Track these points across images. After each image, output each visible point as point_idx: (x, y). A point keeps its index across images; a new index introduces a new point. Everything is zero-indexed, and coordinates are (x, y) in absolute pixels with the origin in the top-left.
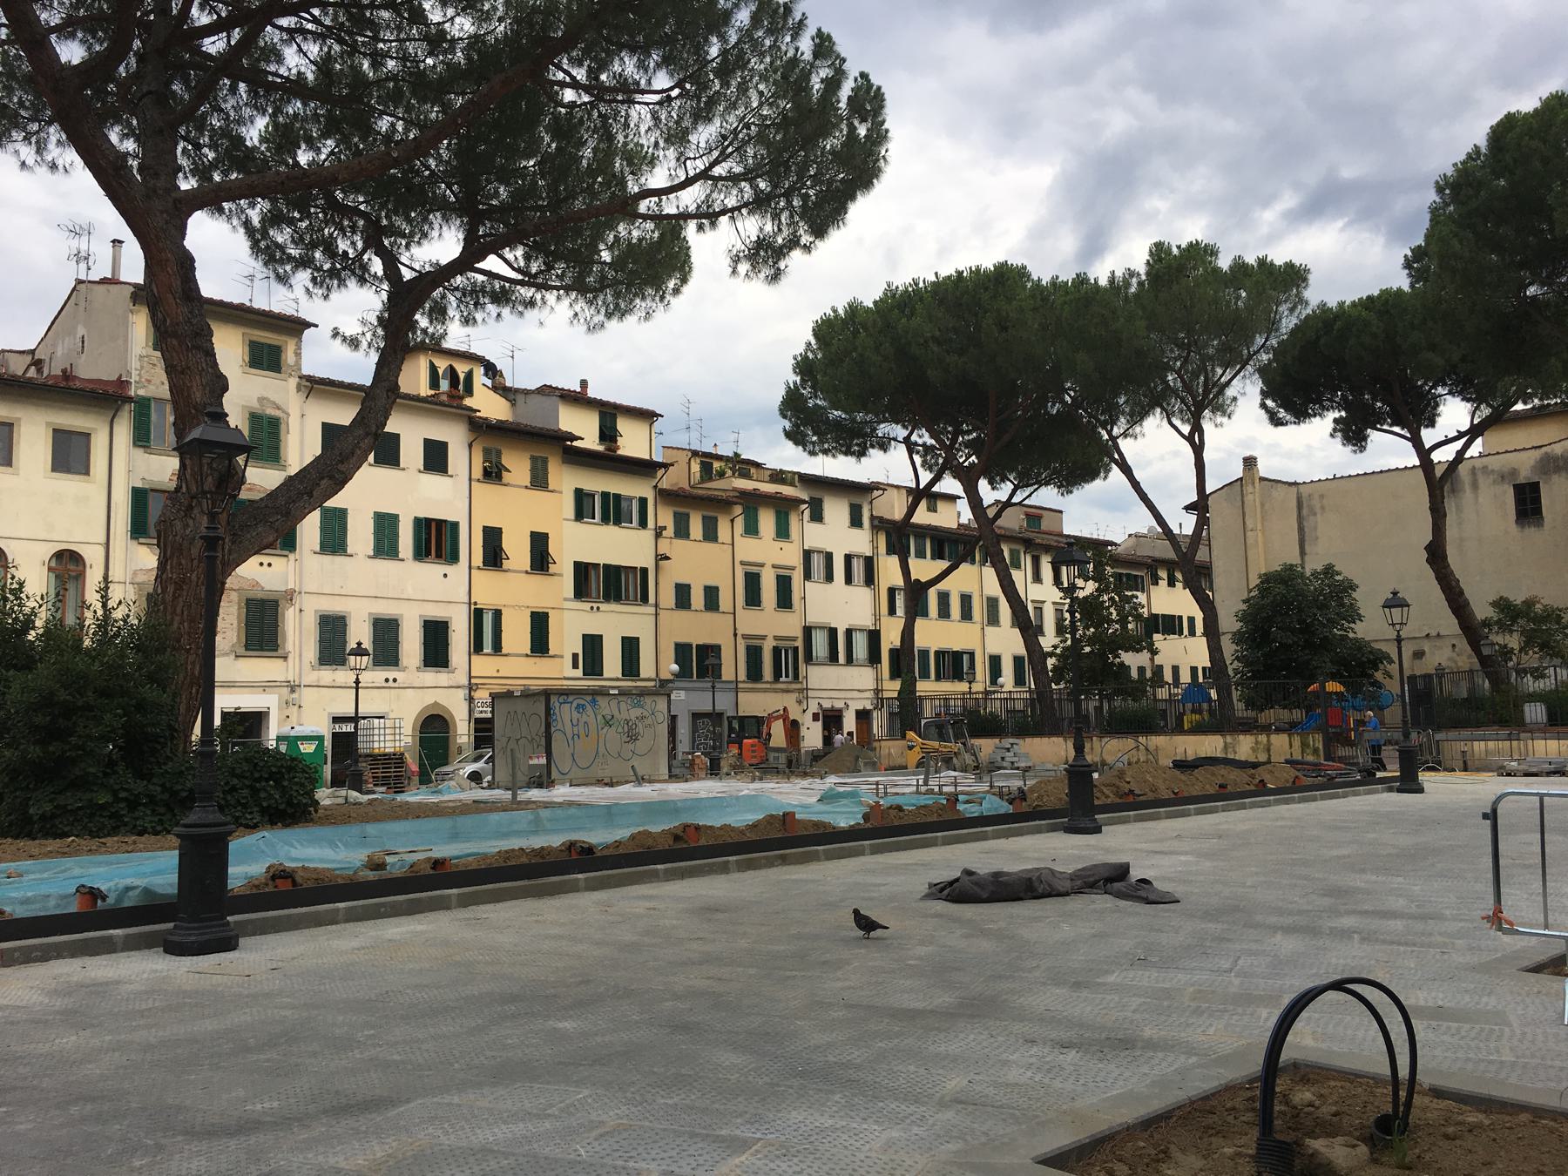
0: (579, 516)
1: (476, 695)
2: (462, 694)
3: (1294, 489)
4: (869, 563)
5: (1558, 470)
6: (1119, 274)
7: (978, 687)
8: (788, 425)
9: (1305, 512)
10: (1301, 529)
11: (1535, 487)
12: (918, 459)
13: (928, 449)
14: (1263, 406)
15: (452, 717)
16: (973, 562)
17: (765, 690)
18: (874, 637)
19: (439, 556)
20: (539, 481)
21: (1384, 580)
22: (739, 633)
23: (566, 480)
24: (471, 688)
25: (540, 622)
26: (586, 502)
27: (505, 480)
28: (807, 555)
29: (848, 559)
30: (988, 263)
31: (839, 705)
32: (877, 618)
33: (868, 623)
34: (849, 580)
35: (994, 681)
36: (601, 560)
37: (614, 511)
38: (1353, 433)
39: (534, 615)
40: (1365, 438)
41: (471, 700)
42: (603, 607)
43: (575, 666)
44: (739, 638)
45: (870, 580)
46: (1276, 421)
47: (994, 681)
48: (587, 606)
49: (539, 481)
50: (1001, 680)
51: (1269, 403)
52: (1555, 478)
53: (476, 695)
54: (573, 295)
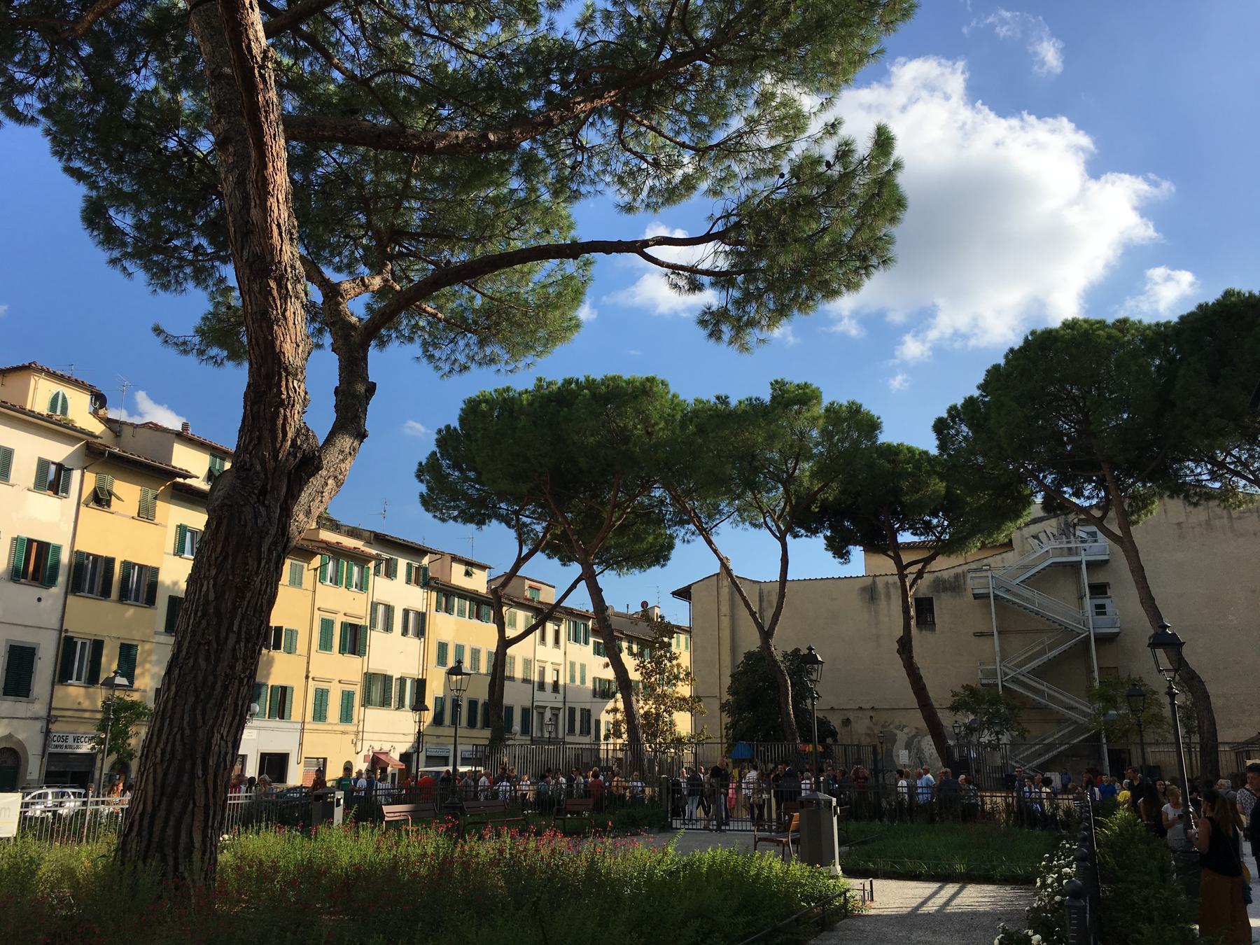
0: (1105, 613)
1: (53, 727)
2: (39, 726)
3: (757, 587)
4: (421, 618)
5: (945, 590)
11: (930, 601)
15: (26, 752)
17: (327, 731)
18: (420, 685)
19: (91, 591)
20: (146, 513)
21: (857, 671)
22: (311, 675)
24: (50, 719)
27: (113, 509)
28: (374, 606)
29: (406, 612)
30: (332, 400)
31: (386, 748)
32: (424, 669)
33: (414, 671)
34: (405, 632)
38: (839, 548)
39: (123, 646)
40: (848, 553)
41: (47, 733)
45: (421, 632)
49: (146, 513)
52: (943, 595)
53: (53, 727)
54: (743, 199)
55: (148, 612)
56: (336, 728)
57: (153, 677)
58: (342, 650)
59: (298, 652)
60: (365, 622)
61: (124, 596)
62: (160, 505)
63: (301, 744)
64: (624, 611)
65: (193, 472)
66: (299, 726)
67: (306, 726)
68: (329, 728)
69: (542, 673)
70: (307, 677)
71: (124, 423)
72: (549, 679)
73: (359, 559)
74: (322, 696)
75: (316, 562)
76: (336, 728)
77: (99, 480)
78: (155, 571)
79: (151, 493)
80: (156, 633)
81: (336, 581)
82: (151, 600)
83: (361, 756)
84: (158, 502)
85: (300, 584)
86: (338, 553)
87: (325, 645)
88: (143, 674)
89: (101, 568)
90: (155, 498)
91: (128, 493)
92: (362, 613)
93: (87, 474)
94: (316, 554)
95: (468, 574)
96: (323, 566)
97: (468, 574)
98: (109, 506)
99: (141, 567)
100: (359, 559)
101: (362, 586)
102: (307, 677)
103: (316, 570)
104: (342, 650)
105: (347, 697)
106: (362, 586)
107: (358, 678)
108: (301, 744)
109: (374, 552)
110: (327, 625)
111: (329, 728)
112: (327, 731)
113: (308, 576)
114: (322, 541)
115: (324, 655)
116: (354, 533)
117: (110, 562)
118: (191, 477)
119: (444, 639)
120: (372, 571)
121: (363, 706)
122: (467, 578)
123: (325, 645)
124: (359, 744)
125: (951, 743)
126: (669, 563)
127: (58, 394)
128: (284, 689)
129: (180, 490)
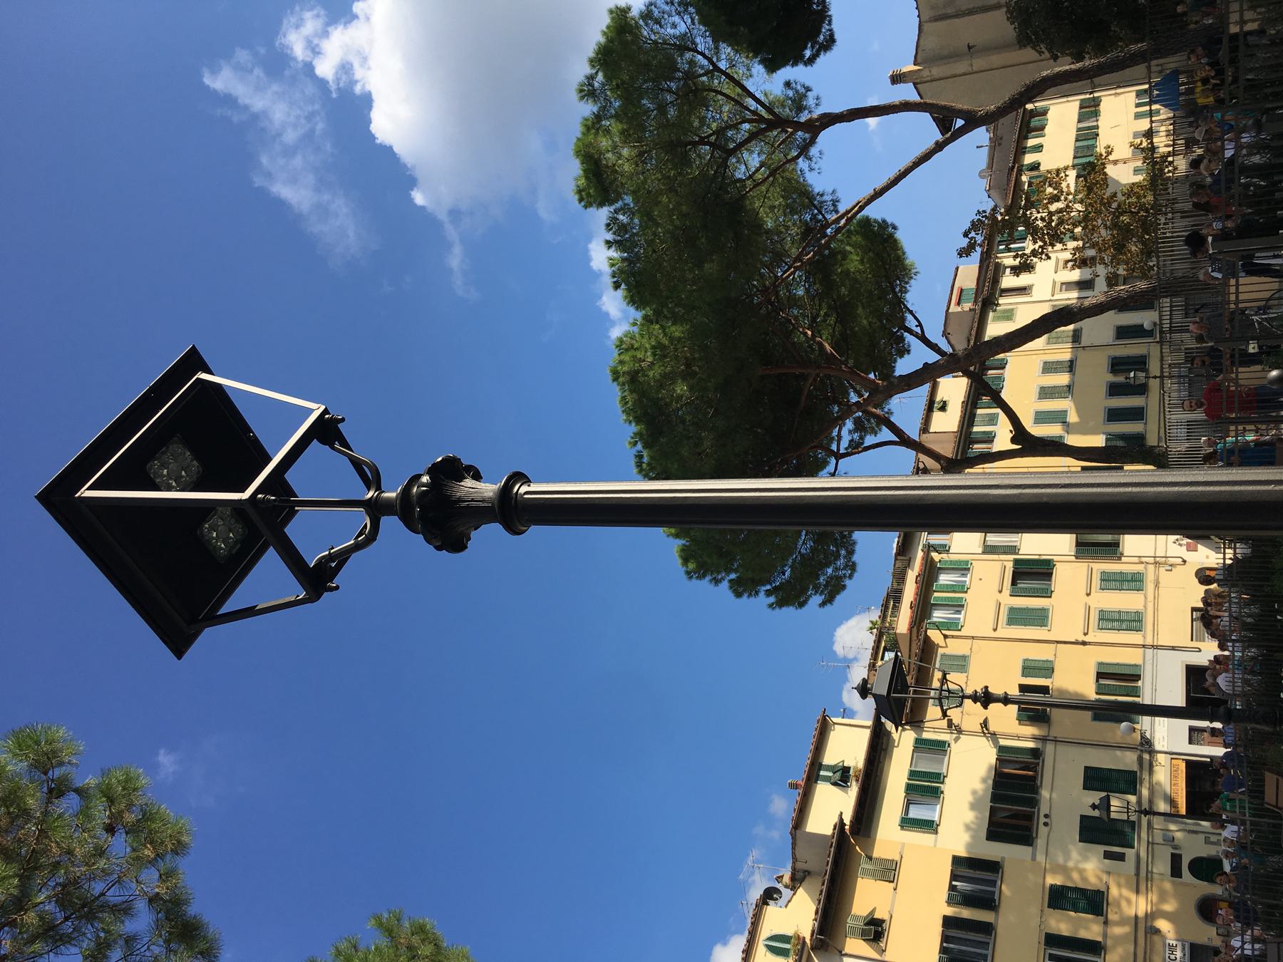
3: (926, 27)
6: (610, 236)
7: (1155, 351)
8: (816, 599)
9: (950, 11)
10: (971, 12)
12: (870, 440)
13: (860, 427)
14: (811, 61)
16: (1191, 195)
17: (1156, 610)
20: (889, 871)
23: (889, 833)
25: (1059, 898)
26: (1024, 568)
27: (886, 917)
35: (1149, 334)
36: (940, 929)
37: (925, 787)
42: (1044, 809)
43: (1121, 857)
44: (1087, 639)
46: (831, 41)
47: (1149, 334)
48: (1043, 830)
50: (1147, 326)
51: (808, 53)
55: (1008, 869)
56: (1150, 597)
57: (1086, 859)
58: (1047, 594)
59: (1051, 658)
60: (1008, 561)
61: (987, 901)
62: (877, 853)
63: (1173, 648)
64: (985, 151)
65: (836, 820)
66: (1149, 651)
67: (1149, 641)
68: (1150, 606)
69: (1068, 286)
70: (1084, 643)
71: (794, 869)
72: (1075, 275)
73: (930, 573)
74: (1110, 620)
75: (935, 635)
76: (1150, 597)
77: (854, 935)
78: (957, 860)
79: (865, 865)
80: (1034, 858)
81: (958, 606)
82: (993, 867)
83: (1189, 556)
84: (875, 855)
85: (964, 658)
86: (923, 608)
87: (1039, 618)
88: (1081, 872)
89: (953, 933)
90: (870, 858)
91: (867, 896)
92: (998, 565)
93: (847, 950)
94: (927, 638)
95: (943, 408)
96: (938, 626)
97: (943, 408)
98: (883, 921)
99: (954, 877)
100: (930, 573)
101: (963, 568)
102: (1084, 643)
103: (946, 637)
104: (1047, 594)
105: (1112, 582)
106: (963, 568)
107: (1082, 567)
108: (1173, 648)
109: (920, 554)
110: (1017, 617)
111: (1150, 606)
112: (1156, 610)
113: (954, 647)
114: (911, 629)
115: (1056, 619)
116: (900, 577)
117: (948, 922)
118: (841, 820)
119: (1035, 392)
120: (944, 556)
121: (1120, 558)
122: (949, 408)
123: (1039, 618)
124: (1171, 561)
125: (1132, 374)
126: (889, 221)
127: (767, 946)
128: (1100, 675)
129: (859, 830)
